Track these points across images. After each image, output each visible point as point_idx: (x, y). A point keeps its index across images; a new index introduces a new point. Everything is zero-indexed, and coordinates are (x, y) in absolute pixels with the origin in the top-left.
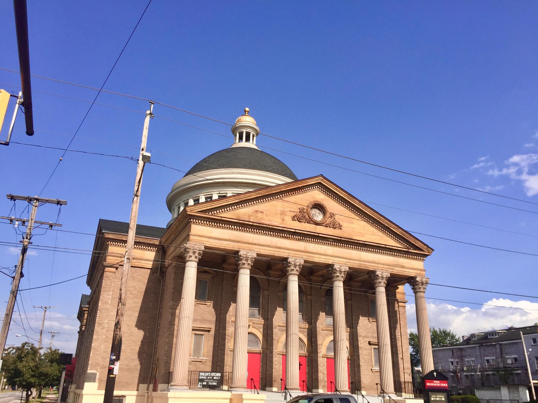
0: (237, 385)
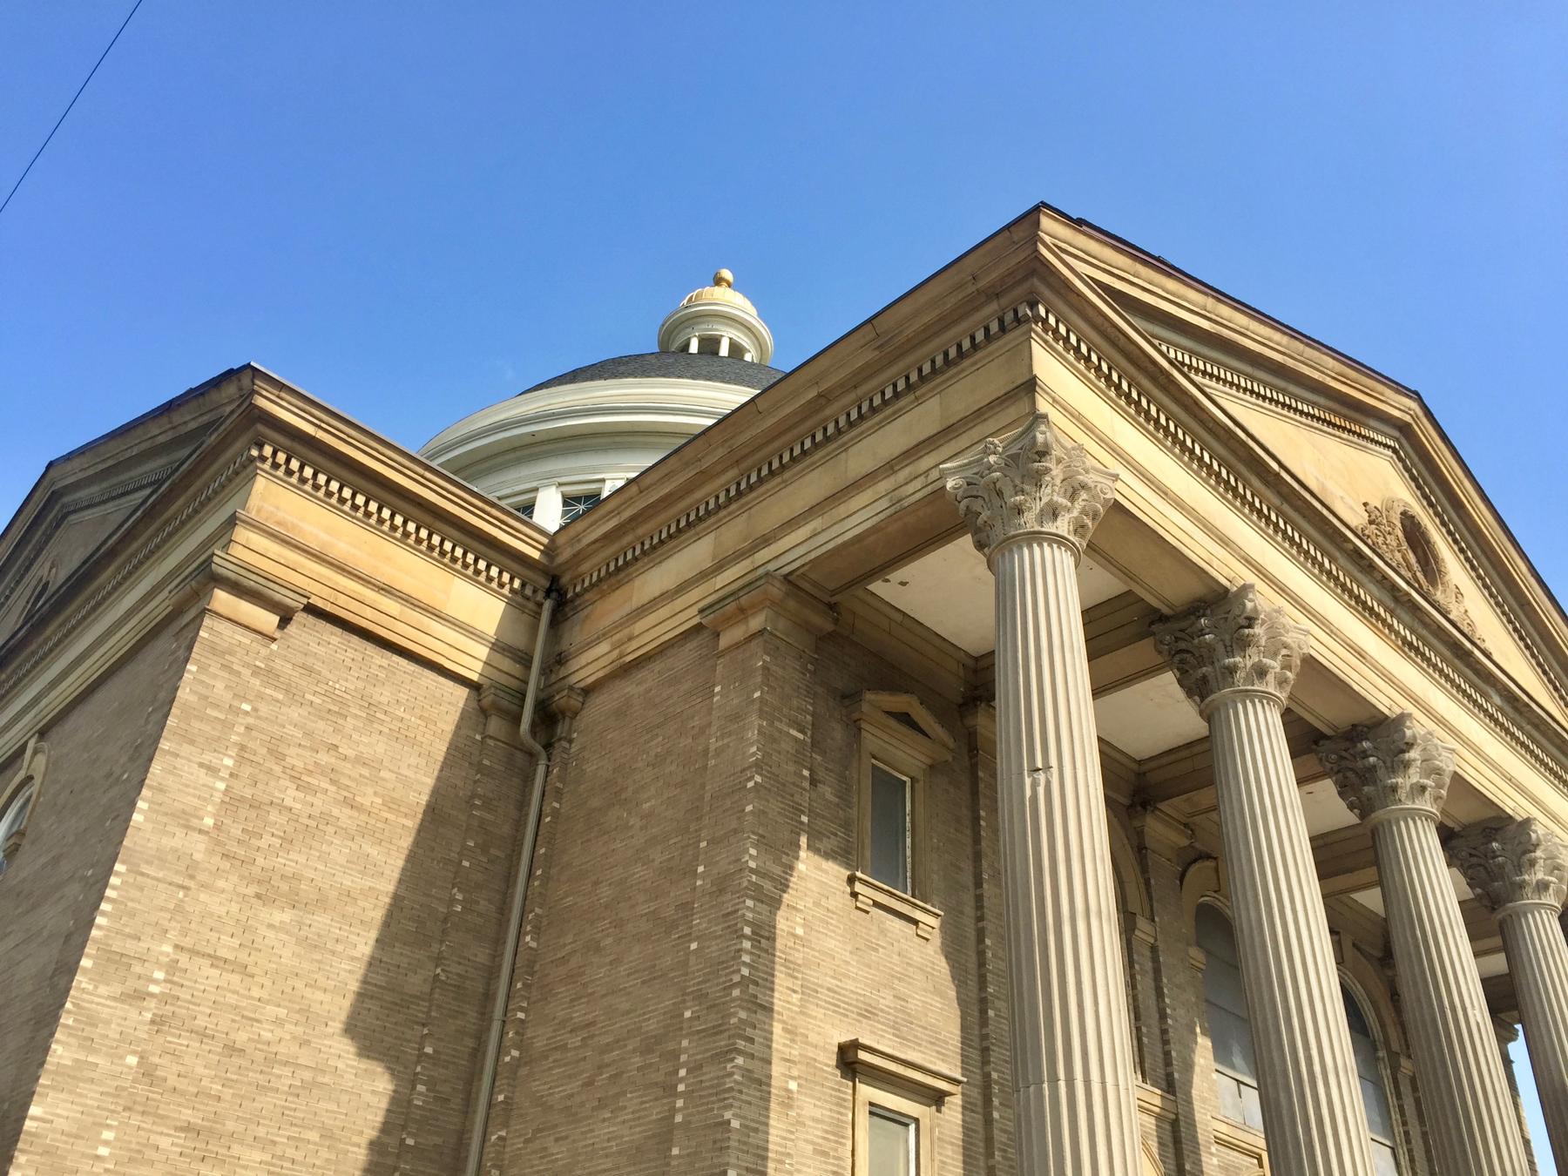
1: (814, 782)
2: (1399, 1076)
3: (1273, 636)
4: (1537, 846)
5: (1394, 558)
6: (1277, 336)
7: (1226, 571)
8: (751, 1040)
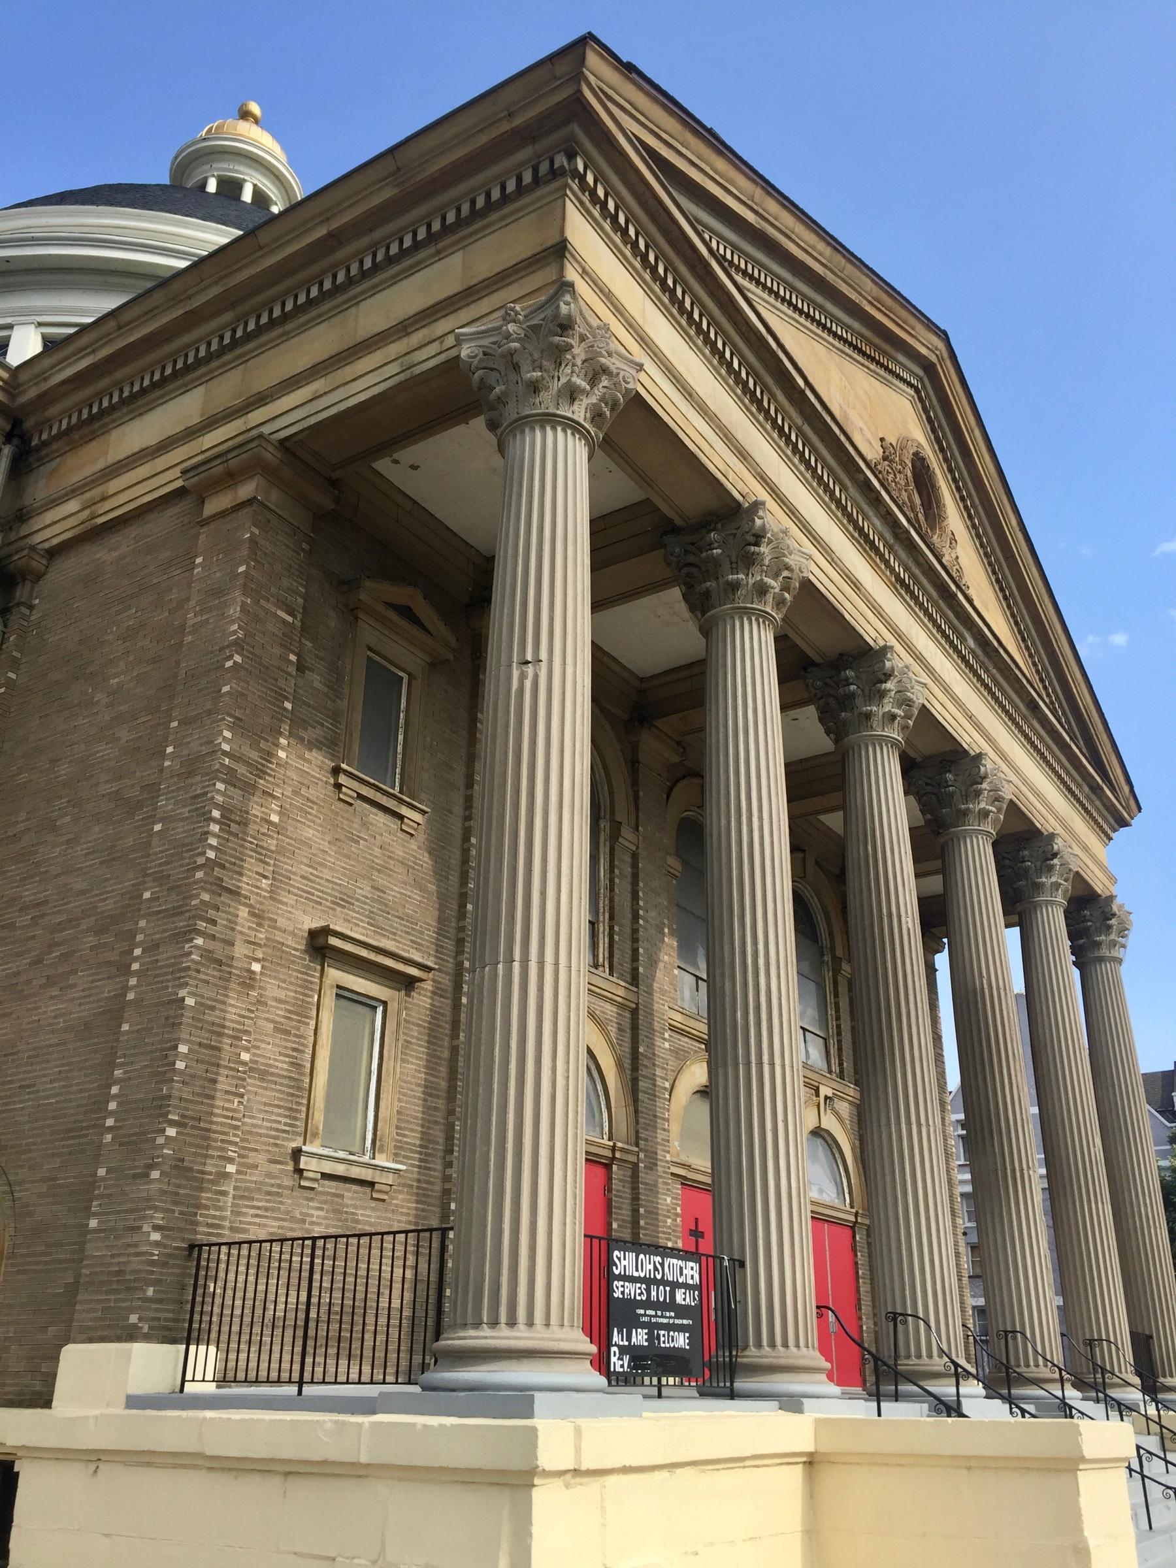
1: (301, 668)
2: (840, 978)
3: (778, 556)
4: (985, 777)
5: (900, 498)
6: (821, 246)
7: (740, 485)
8: (213, 922)
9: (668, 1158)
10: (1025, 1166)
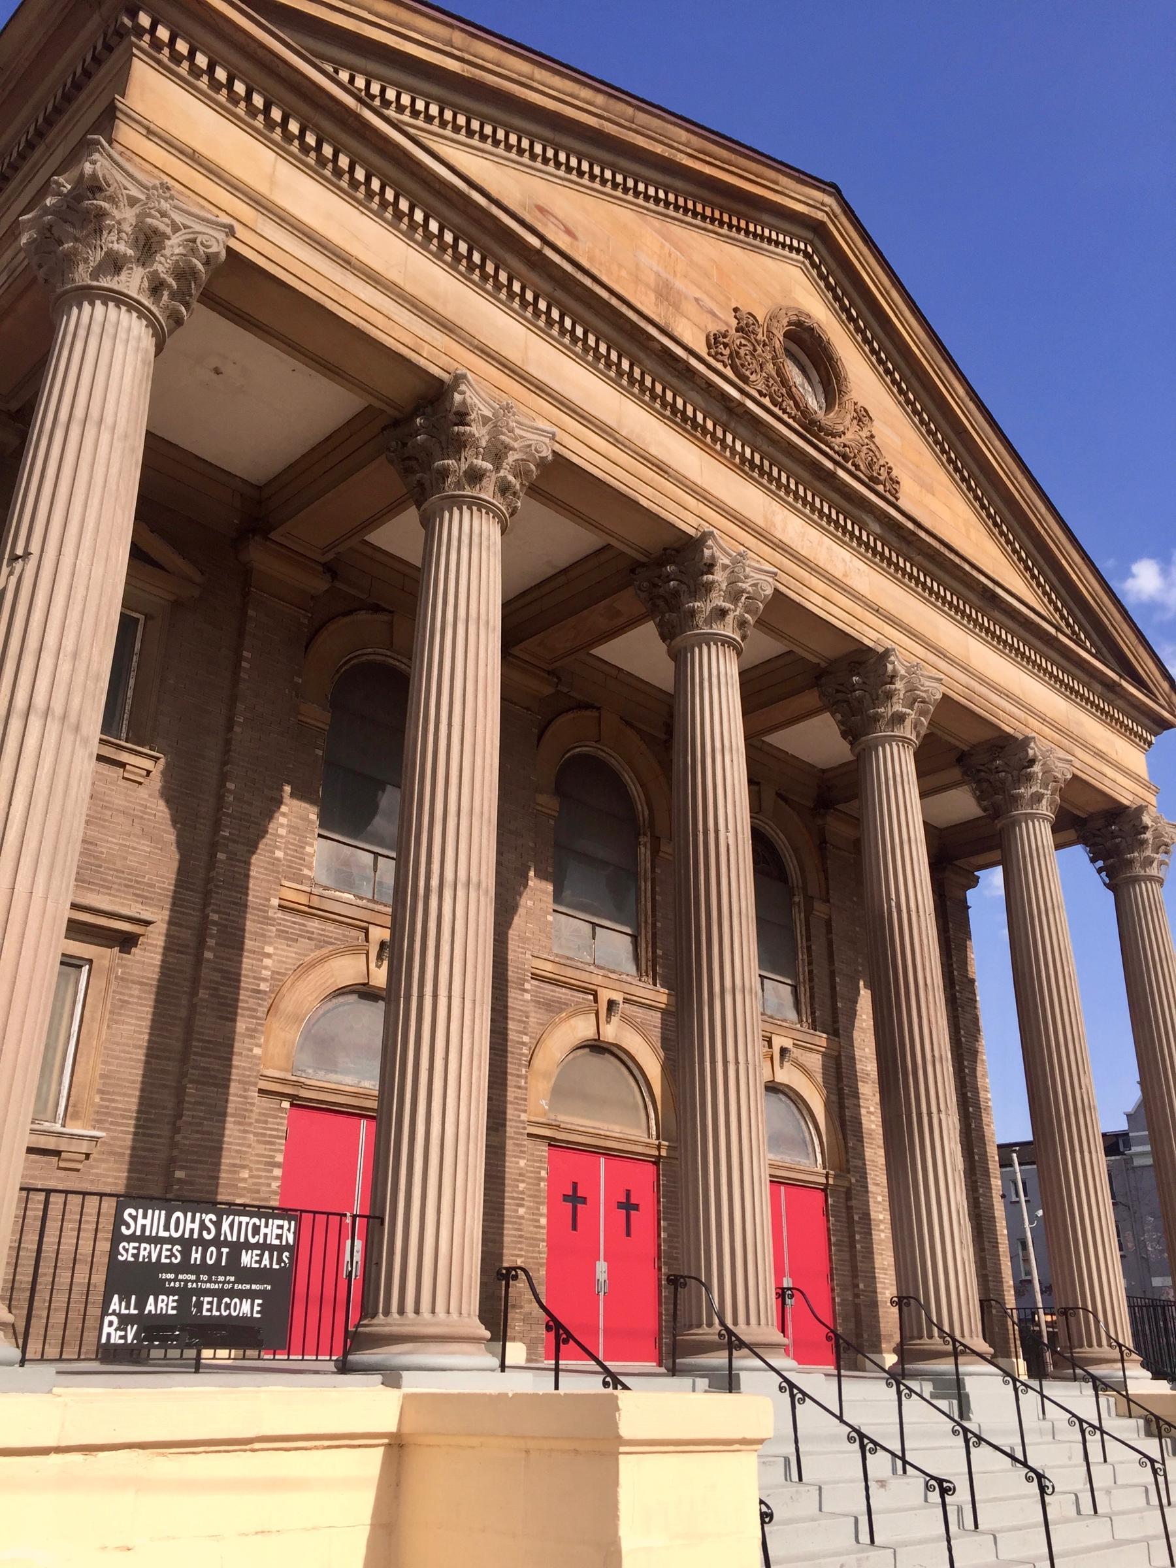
0: (426, 1323)
9: (524, 1117)
10: (934, 1109)
